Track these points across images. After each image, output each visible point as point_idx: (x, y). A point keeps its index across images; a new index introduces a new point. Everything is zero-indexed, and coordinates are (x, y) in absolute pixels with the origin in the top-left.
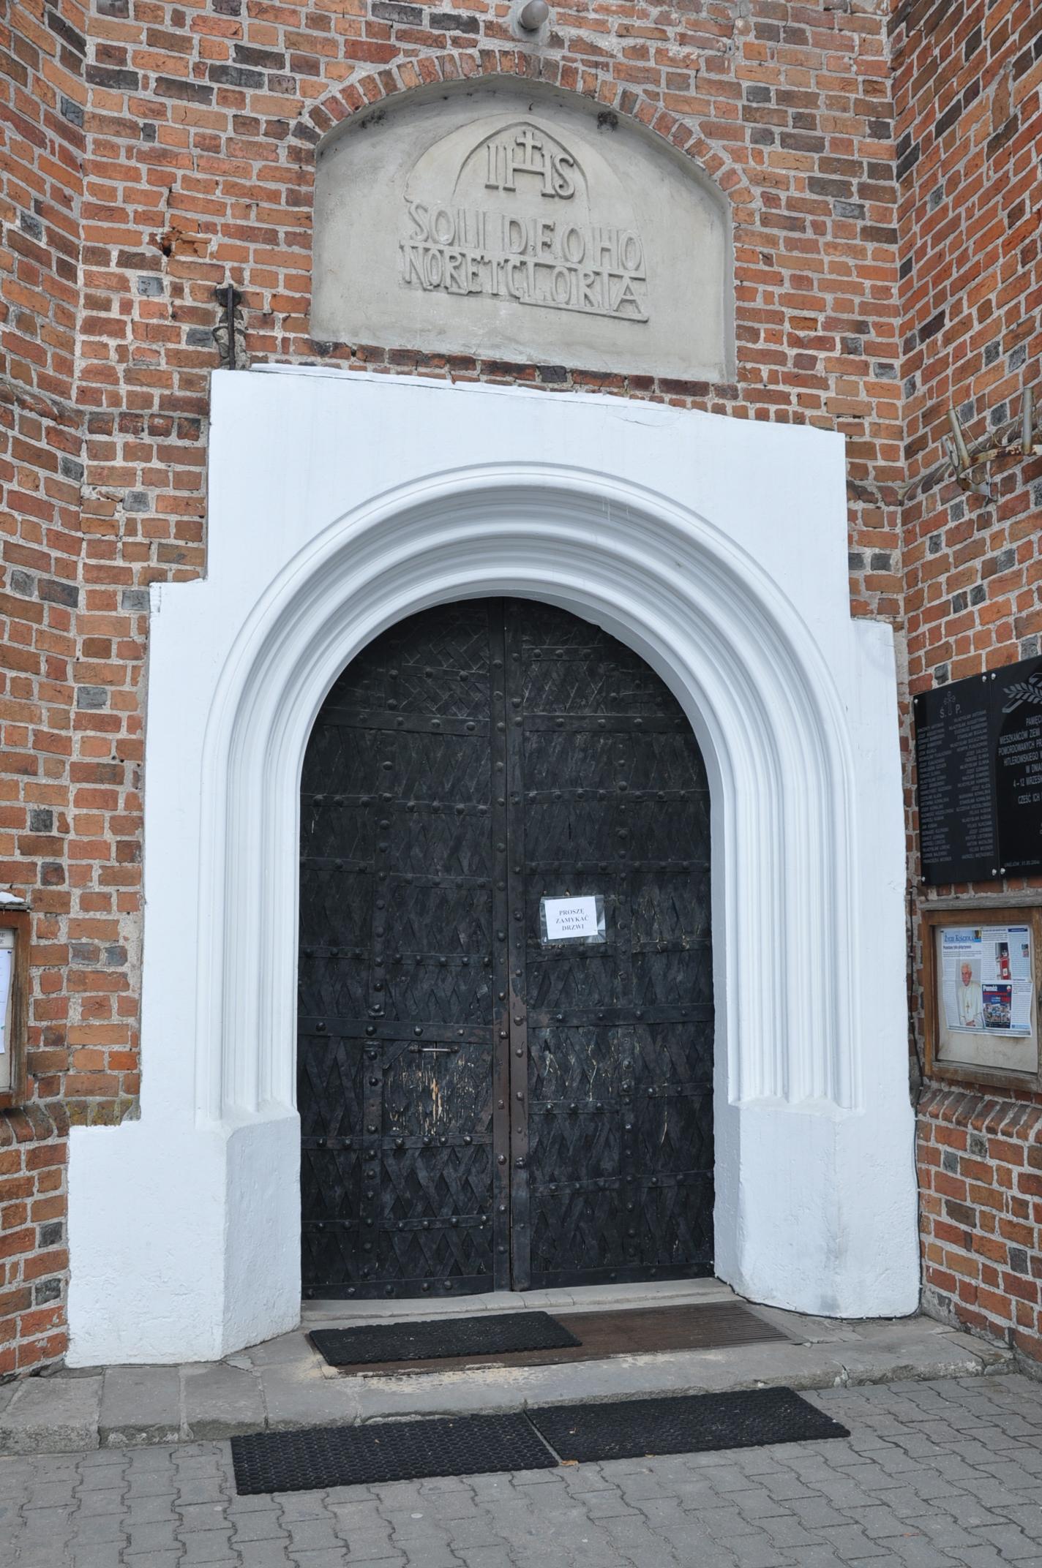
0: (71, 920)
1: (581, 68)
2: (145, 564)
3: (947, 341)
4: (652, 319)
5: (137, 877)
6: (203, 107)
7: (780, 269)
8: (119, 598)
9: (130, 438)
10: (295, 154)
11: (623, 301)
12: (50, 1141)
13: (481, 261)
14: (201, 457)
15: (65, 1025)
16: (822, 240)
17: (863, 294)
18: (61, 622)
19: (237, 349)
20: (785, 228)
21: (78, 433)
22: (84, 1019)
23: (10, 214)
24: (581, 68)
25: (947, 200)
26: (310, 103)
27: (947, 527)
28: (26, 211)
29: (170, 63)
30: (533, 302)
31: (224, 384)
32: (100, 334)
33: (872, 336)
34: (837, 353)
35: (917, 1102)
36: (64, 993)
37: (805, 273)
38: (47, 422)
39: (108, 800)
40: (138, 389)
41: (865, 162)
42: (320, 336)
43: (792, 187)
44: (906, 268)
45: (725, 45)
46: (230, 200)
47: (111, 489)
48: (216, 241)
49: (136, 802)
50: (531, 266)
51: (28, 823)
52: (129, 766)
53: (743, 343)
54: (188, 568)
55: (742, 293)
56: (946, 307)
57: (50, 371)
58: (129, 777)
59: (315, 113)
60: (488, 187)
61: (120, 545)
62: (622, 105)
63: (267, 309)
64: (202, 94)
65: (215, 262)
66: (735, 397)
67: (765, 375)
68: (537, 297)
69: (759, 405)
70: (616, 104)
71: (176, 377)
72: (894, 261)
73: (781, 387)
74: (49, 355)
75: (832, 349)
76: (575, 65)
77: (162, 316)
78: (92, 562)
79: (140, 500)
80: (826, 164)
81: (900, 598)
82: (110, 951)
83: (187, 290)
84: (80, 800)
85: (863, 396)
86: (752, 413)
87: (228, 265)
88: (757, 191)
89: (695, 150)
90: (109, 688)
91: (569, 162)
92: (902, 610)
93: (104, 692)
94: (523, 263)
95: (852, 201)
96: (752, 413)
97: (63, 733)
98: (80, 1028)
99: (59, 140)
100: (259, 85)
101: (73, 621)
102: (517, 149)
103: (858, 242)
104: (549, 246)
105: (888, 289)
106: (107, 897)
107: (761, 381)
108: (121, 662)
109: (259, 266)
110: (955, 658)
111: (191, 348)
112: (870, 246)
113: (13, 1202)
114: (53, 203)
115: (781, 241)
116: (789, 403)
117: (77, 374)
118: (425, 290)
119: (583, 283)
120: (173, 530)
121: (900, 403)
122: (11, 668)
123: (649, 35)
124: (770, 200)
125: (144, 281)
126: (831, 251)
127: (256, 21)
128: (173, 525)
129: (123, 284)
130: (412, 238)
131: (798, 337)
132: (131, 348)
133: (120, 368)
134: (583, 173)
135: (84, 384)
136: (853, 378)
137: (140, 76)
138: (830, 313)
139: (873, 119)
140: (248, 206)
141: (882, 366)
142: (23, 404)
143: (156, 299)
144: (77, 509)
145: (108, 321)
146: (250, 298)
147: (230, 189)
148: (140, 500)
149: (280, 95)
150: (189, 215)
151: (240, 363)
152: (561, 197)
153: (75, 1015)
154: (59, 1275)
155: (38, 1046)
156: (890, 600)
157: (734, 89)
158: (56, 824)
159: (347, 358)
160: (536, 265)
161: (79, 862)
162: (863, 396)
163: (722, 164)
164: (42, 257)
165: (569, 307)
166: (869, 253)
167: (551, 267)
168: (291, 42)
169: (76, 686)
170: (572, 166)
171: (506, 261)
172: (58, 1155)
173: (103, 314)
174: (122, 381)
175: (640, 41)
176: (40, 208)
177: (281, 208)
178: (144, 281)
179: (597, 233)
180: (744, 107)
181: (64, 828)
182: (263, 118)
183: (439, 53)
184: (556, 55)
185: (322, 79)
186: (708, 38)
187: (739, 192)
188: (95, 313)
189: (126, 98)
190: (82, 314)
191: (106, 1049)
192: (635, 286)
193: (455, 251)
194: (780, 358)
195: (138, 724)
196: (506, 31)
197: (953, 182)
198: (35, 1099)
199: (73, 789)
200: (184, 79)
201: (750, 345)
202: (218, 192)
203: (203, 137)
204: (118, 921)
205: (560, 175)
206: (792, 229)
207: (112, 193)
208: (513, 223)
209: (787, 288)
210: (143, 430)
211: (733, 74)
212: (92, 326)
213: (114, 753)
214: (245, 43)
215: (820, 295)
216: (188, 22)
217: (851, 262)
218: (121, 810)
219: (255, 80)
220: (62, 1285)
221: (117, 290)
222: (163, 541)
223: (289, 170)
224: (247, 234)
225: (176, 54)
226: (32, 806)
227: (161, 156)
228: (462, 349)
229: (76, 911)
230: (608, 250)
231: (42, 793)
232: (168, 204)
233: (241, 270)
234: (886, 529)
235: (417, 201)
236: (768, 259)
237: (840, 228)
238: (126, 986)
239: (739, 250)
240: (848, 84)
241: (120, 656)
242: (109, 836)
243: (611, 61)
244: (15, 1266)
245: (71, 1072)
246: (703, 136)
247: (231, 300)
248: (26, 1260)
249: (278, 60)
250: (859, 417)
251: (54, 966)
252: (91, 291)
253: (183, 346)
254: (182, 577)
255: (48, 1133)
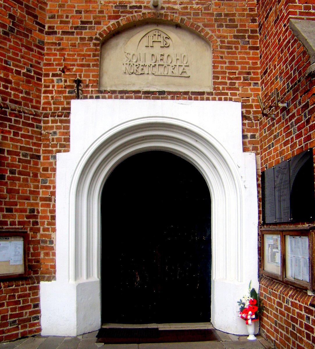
0: (41, 234)
1: (169, 14)
2: (56, 149)
3: (269, 76)
4: (191, 77)
5: (54, 224)
6: (72, 36)
7: (225, 60)
8: (50, 157)
9: (53, 118)
10: (95, 45)
11: (182, 72)
12: (35, 285)
13: (144, 66)
14: (68, 122)
15: (40, 258)
16: (237, 51)
17: (249, 65)
18: (36, 164)
19: (80, 94)
20: (226, 49)
21: (40, 118)
22: (44, 257)
23: (23, 68)
24: (169, 14)
25: (267, 38)
26: (98, 32)
27: (267, 127)
28: (28, 67)
29: (65, 28)
30: (158, 75)
31: (75, 104)
32: (47, 94)
33: (252, 75)
34: (242, 81)
35: (260, 281)
36: (39, 251)
37: (233, 60)
38: (31, 116)
39: (48, 206)
40: (56, 106)
41: (250, 29)
42: (102, 89)
43: (229, 38)
44: (261, 57)
45: (209, 3)
46: (79, 58)
47: (48, 131)
48: (75, 68)
49: (54, 206)
50: (157, 65)
51: (28, 212)
52: (53, 197)
53: (215, 80)
54: (66, 149)
55: (214, 67)
56: (268, 66)
57: (34, 104)
58: (53, 200)
59: (100, 34)
60: (146, 46)
61: (50, 144)
62: (181, 22)
63: (87, 83)
64: (72, 33)
65: (75, 73)
66: (212, 95)
67: (221, 88)
68: (159, 73)
69: (219, 96)
70: (179, 22)
71: (65, 102)
72: (258, 55)
73: (226, 91)
74: (34, 100)
75: (240, 80)
76: (168, 13)
77: (62, 88)
78: (44, 149)
79: (55, 133)
80: (238, 31)
81: (259, 146)
82: (50, 241)
83: (68, 81)
84: (42, 206)
85: (249, 92)
86: (217, 99)
87: (78, 74)
88: (219, 40)
89: (201, 31)
90: (48, 179)
91: (169, 38)
92: (259, 149)
93: (47, 180)
94: (155, 65)
95: (246, 40)
96: (217, 99)
97: (37, 190)
98: (43, 259)
99: (37, 49)
100: (86, 29)
101: (40, 163)
102: (154, 36)
103: (248, 51)
104: (163, 60)
105: (257, 62)
106: (48, 228)
107: (220, 90)
108: (51, 172)
109: (86, 73)
110: (269, 162)
111: (69, 95)
112: (251, 52)
113: (25, 298)
114: (35, 64)
115: (226, 52)
116: (228, 95)
117: (42, 104)
118: (130, 74)
119: (171, 68)
120: (63, 140)
121: (260, 93)
122: (22, 175)
123: (188, 4)
124: (223, 42)
125: (57, 80)
126: (240, 54)
127: (86, 14)
128: (63, 139)
129: (53, 81)
130: (126, 62)
131: (230, 77)
132: (54, 96)
133: (52, 102)
134: (172, 41)
135: (43, 106)
136: (247, 87)
137: (57, 32)
138: (240, 70)
139: (252, 18)
140: (83, 59)
141: (255, 83)
142: (25, 113)
143: (60, 84)
144: (40, 136)
145: (49, 90)
146: (83, 81)
147: (79, 55)
148: (55, 133)
149: (91, 31)
150: (69, 63)
151: (80, 97)
152: (166, 47)
153: (42, 256)
154: (39, 315)
155: (32, 263)
156: (256, 147)
157: (212, 14)
158: (36, 212)
159: (108, 93)
160: (159, 65)
161: (42, 220)
162: (249, 92)
163: (209, 34)
164: (33, 77)
165: (168, 75)
166: (251, 53)
167: (163, 65)
168: (94, 18)
169: (41, 179)
170: (169, 39)
171: (151, 65)
172: (37, 288)
173: (48, 89)
174: (52, 104)
175: (185, 5)
176: (32, 66)
177: (91, 58)
178: (57, 80)
179: (175, 55)
180: (215, 19)
181: (38, 212)
182: (87, 37)
183: (131, 15)
184: (163, 12)
185: (102, 26)
186: (204, 2)
187: (214, 41)
188: (46, 89)
189: (54, 37)
190: (43, 89)
191: (49, 264)
192: (186, 68)
193: (137, 64)
194: (225, 83)
195: (54, 187)
196: (149, 7)
197: (268, 33)
198: (32, 275)
199: (40, 203)
200: (68, 31)
201: (217, 81)
202: (76, 56)
203: (72, 43)
204: (51, 234)
205: (165, 41)
206: (228, 49)
207: (50, 60)
208: (153, 55)
209: (227, 65)
210: (56, 116)
211: (211, 11)
212: (45, 92)
213: (49, 194)
214: (83, 20)
215: (237, 66)
216: (69, 17)
217: (246, 56)
218: (51, 208)
219: (85, 28)
220: (39, 317)
221: (51, 83)
222: (61, 143)
223: (93, 49)
224: (82, 65)
225: (66, 25)
226: (29, 207)
227: (62, 49)
228: (139, 88)
229: (41, 232)
230: (178, 59)
231: (32, 204)
232: (64, 61)
233: (81, 75)
234: (255, 127)
235: (127, 52)
236: (222, 57)
237: (242, 48)
238: (53, 249)
239: (213, 56)
240: (244, 10)
241: (51, 171)
242: (49, 214)
243: (178, 11)
244: (26, 313)
245: (41, 269)
246: (203, 27)
247: (78, 82)
248: (29, 311)
249: (91, 23)
250: (248, 98)
251: (36, 245)
252: (45, 84)
253: (67, 95)
254: (65, 151)
255: (34, 283)
